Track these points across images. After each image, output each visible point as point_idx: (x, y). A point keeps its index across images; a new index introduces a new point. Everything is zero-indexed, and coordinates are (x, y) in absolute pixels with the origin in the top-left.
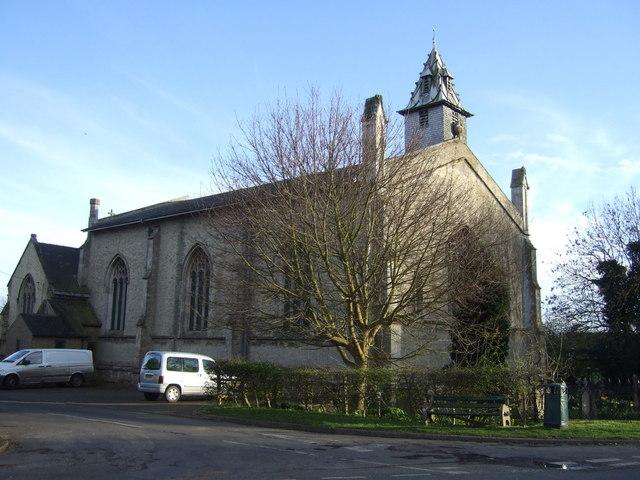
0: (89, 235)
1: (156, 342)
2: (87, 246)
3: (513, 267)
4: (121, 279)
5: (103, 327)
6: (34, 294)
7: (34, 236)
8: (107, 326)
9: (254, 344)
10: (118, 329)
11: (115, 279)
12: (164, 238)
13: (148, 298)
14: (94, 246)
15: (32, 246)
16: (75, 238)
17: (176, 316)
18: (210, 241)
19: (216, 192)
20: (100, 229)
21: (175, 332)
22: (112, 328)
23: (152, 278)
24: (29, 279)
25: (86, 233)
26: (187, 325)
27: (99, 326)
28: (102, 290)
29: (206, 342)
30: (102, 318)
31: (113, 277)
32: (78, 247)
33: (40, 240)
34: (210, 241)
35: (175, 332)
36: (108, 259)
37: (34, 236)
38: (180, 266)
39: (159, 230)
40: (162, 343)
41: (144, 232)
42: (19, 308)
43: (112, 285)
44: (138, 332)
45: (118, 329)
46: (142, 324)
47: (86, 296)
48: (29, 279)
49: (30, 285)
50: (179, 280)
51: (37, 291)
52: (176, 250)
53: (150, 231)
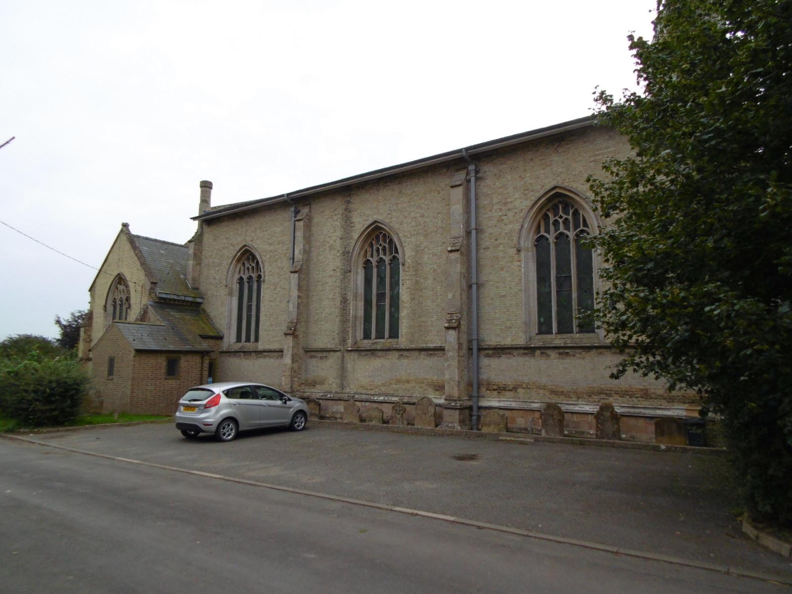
0: (201, 227)
1: (312, 357)
2: (197, 239)
3: (738, 188)
4: (250, 278)
5: (225, 339)
6: (128, 299)
7: (125, 225)
8: (230, 339)
9: (488, 356)
10: (248, 339)
11: (241, 279)
12: (316, 219)
13: (299, 297)
14: (207, 238)
15: (124, 238)
16: (181, 229)
17: (344, 321)
18: (351, 322)
19: (589, 113)
20: (211, 219)
21: (344, 341)
22: (239, 339)
23: (302, 271)
24: (120, 279)
25: (196, 223)
26: (360, 334)
27: (221, 338)
28: (223, 292)
29: (396, 354)
30: (225, 333)
31: (237, 276)
32: (183, 243)
33: (134, 230)
34: (351, 322)
35: (344, 341)
36: (232, 252)
37: (125, 225)
38: (346, 254)
39: (310, 211)
40: (321, 358)
41: (289, 213)
42: (106, 317)
43: (236, 287)
44: (288, 344)
45: (248, 339)
46: (292, 332)
47: (199, 300)
48: (120, 279)
49: (121, 287)
50: (346, 272)
51: (133, 294)
52: (339, 233)
53: (297, 212)
